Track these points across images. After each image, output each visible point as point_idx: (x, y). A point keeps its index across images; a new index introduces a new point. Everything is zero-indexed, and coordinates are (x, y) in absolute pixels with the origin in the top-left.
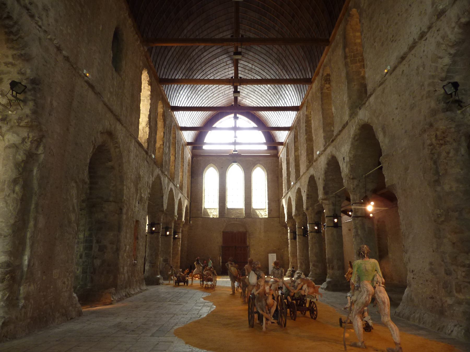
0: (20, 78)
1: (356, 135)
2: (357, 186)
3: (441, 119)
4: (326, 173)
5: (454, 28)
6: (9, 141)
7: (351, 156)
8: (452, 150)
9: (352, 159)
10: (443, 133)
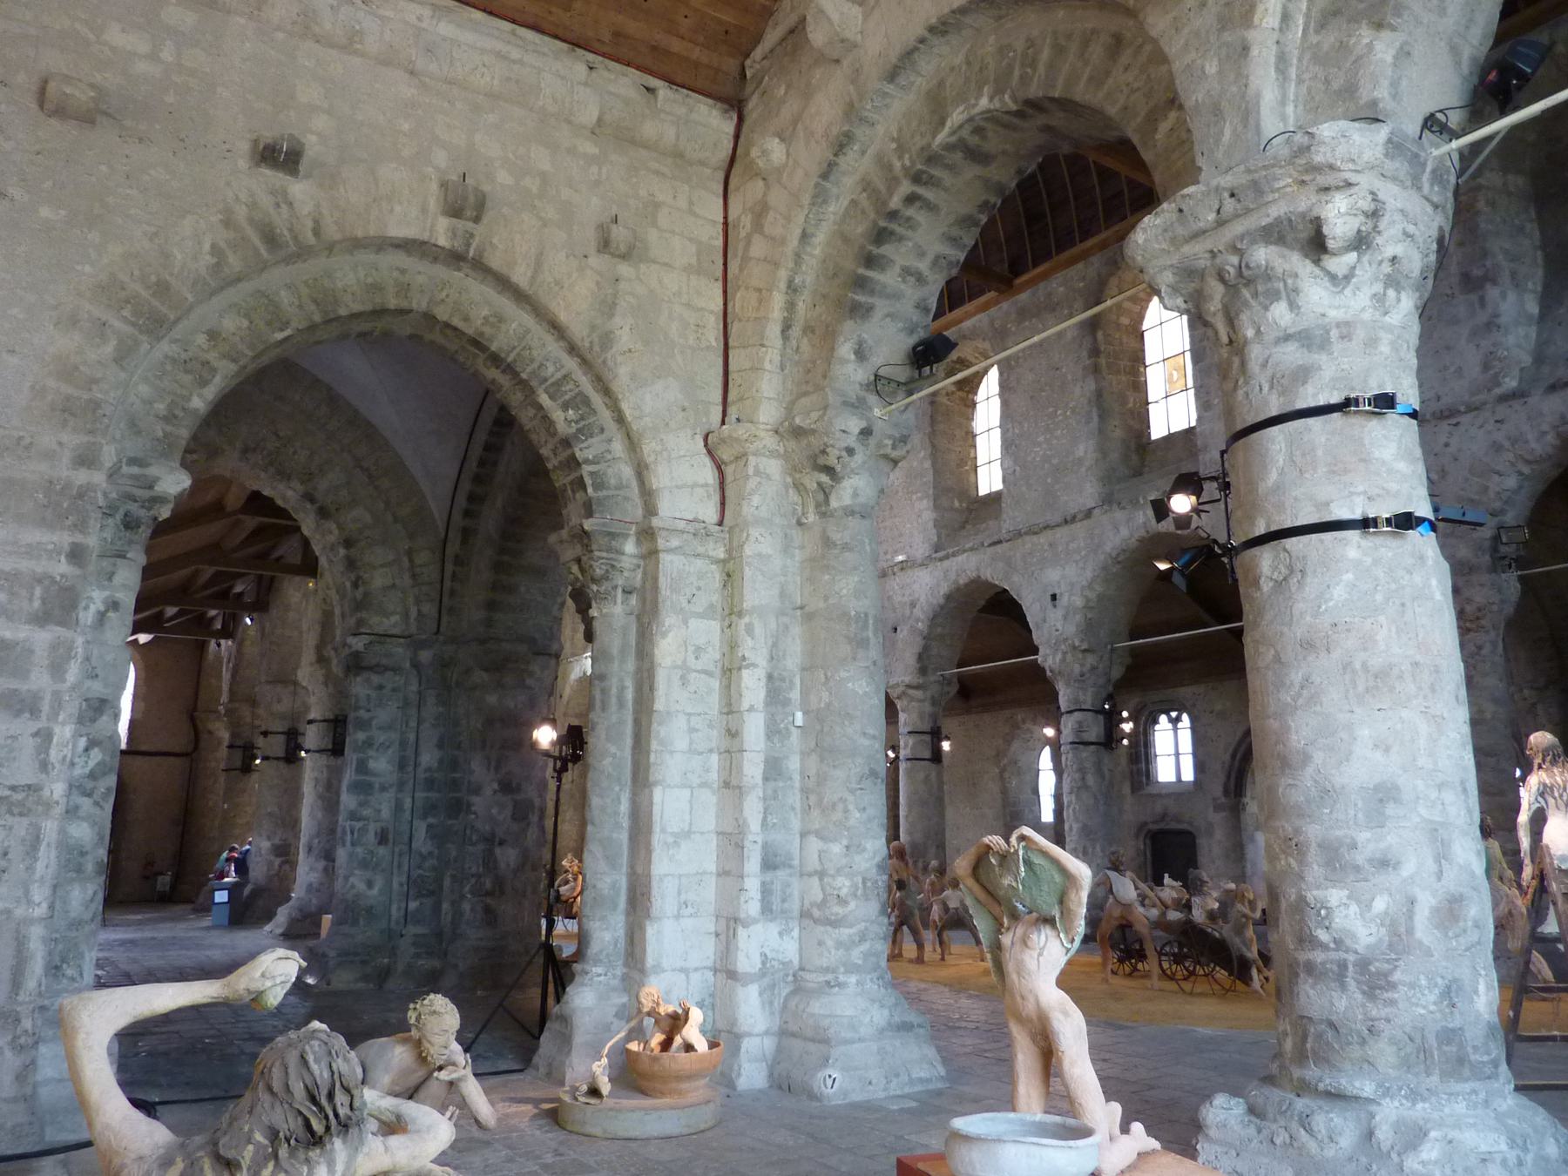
0: (915, 319)
1: (1124, 551)
2: (1093, 668)
3: (1481, 585)
4: (934, 619)
5: (1544, 433)
6: (855, 495)
7: (1092, 595)
8: (1488, 645)
9: (1091, 604)
10: (1479, 610)
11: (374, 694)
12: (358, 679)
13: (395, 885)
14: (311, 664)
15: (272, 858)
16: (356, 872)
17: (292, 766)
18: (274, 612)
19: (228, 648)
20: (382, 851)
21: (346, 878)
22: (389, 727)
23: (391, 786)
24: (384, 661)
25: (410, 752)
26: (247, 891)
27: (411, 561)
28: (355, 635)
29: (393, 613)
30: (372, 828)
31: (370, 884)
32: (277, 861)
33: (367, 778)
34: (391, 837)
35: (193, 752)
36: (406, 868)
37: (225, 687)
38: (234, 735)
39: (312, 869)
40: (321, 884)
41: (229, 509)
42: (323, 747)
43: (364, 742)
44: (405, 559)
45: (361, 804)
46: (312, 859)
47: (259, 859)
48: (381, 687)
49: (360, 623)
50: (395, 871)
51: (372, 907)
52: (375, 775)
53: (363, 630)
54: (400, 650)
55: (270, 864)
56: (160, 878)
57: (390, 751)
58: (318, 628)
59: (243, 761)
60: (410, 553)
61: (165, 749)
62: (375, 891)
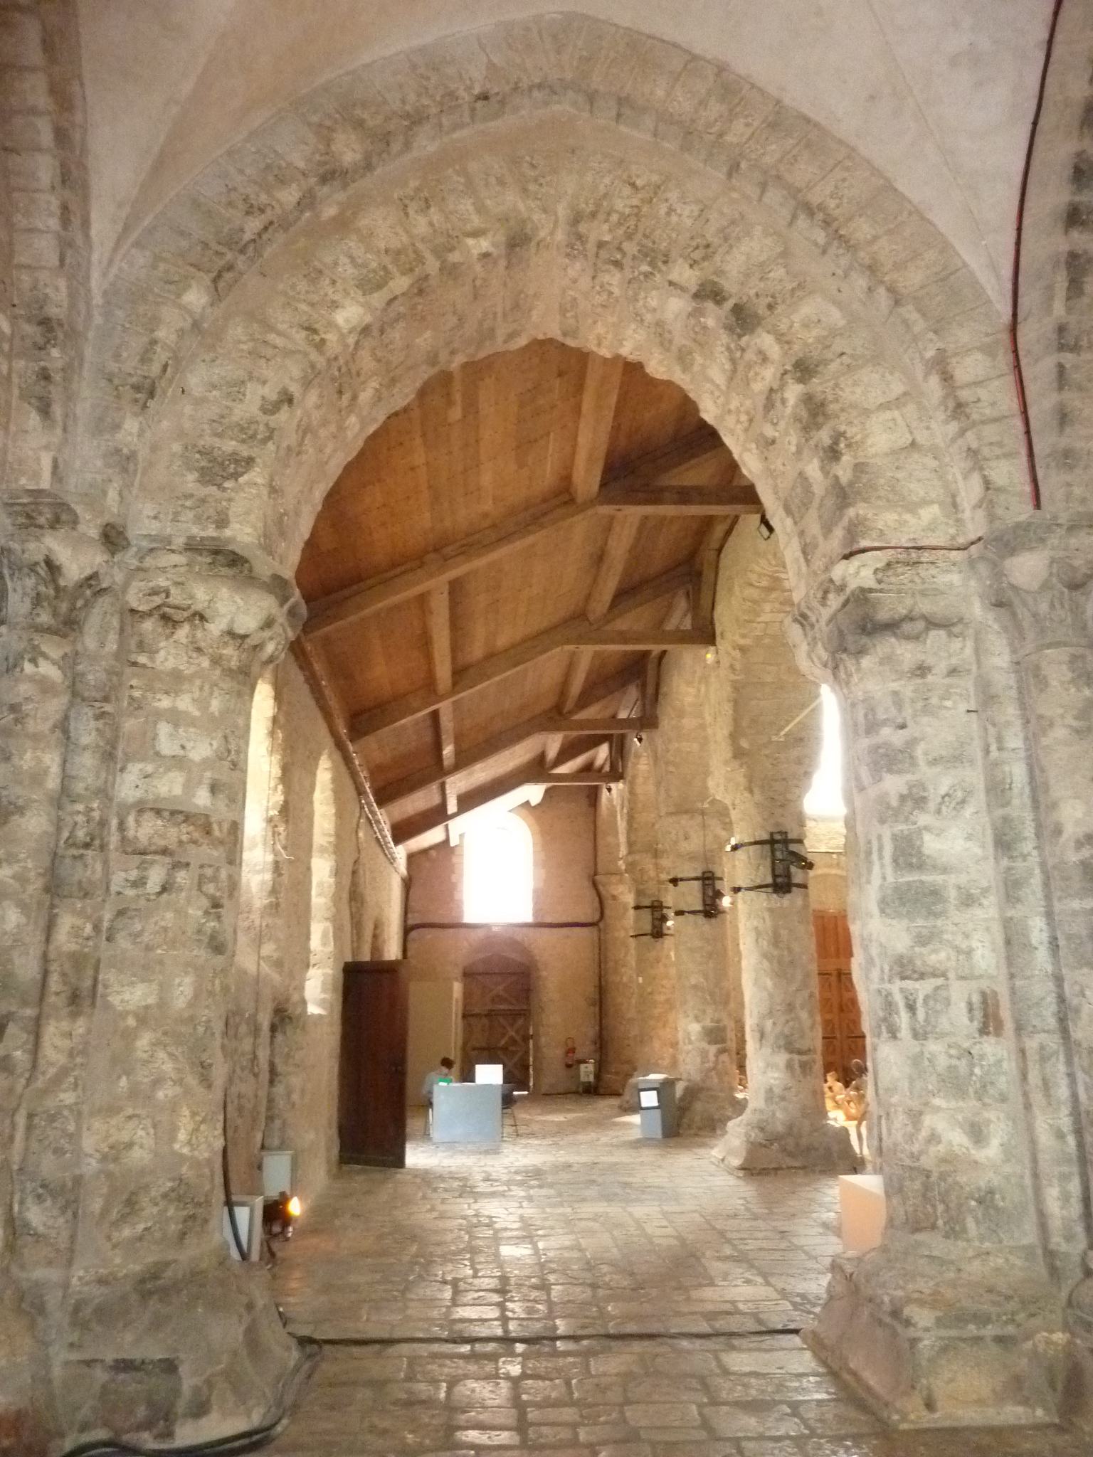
11: (907, 689)
12: (866, 662)
13: (1045, 1138)
14: (726, 763)
15: (704, 1045)
16: (937, 1101)
17: (713, 921)
18: (665, 723)
19: (620, 792)
20: (994, 1050)
21: (915, 1117)
22: (956, 759)
23: (985, 891)
24: (925, 606)
25: (1020, 806)
26: (679, 1089)
27: (947, 378)
28: (847, 557)
29: (925, 502)
30: (960, 994)
31: (977, 1133)
32: (713, 1049)
33: (928, 878)
34: (1006, 1014)
35: (598, 922)
36: (1063, 1092)
37: (622, 839)
38: (639, 893)
39: (769, 1065)
40: (787, 1089)
41: (579, 500)
42: (758, 882)
43: (903, 798)
44: (934, 382)
45: (923, 940)
46: (767, 1050)
47: (690, 1047)
48: (922, 670)
49: (853, 531)
50: (1037, 1098)
51: (991, 1192)
52: (945, 870)
53: (864, 543)
54: (955, 578)
55: (704, 1054)
56: (582, 1066)
57: (968, 811)
58: (728, 708)
59: (654, 926)
60: (942, 367)
61: (570, 920)
62: (992, 1151)
